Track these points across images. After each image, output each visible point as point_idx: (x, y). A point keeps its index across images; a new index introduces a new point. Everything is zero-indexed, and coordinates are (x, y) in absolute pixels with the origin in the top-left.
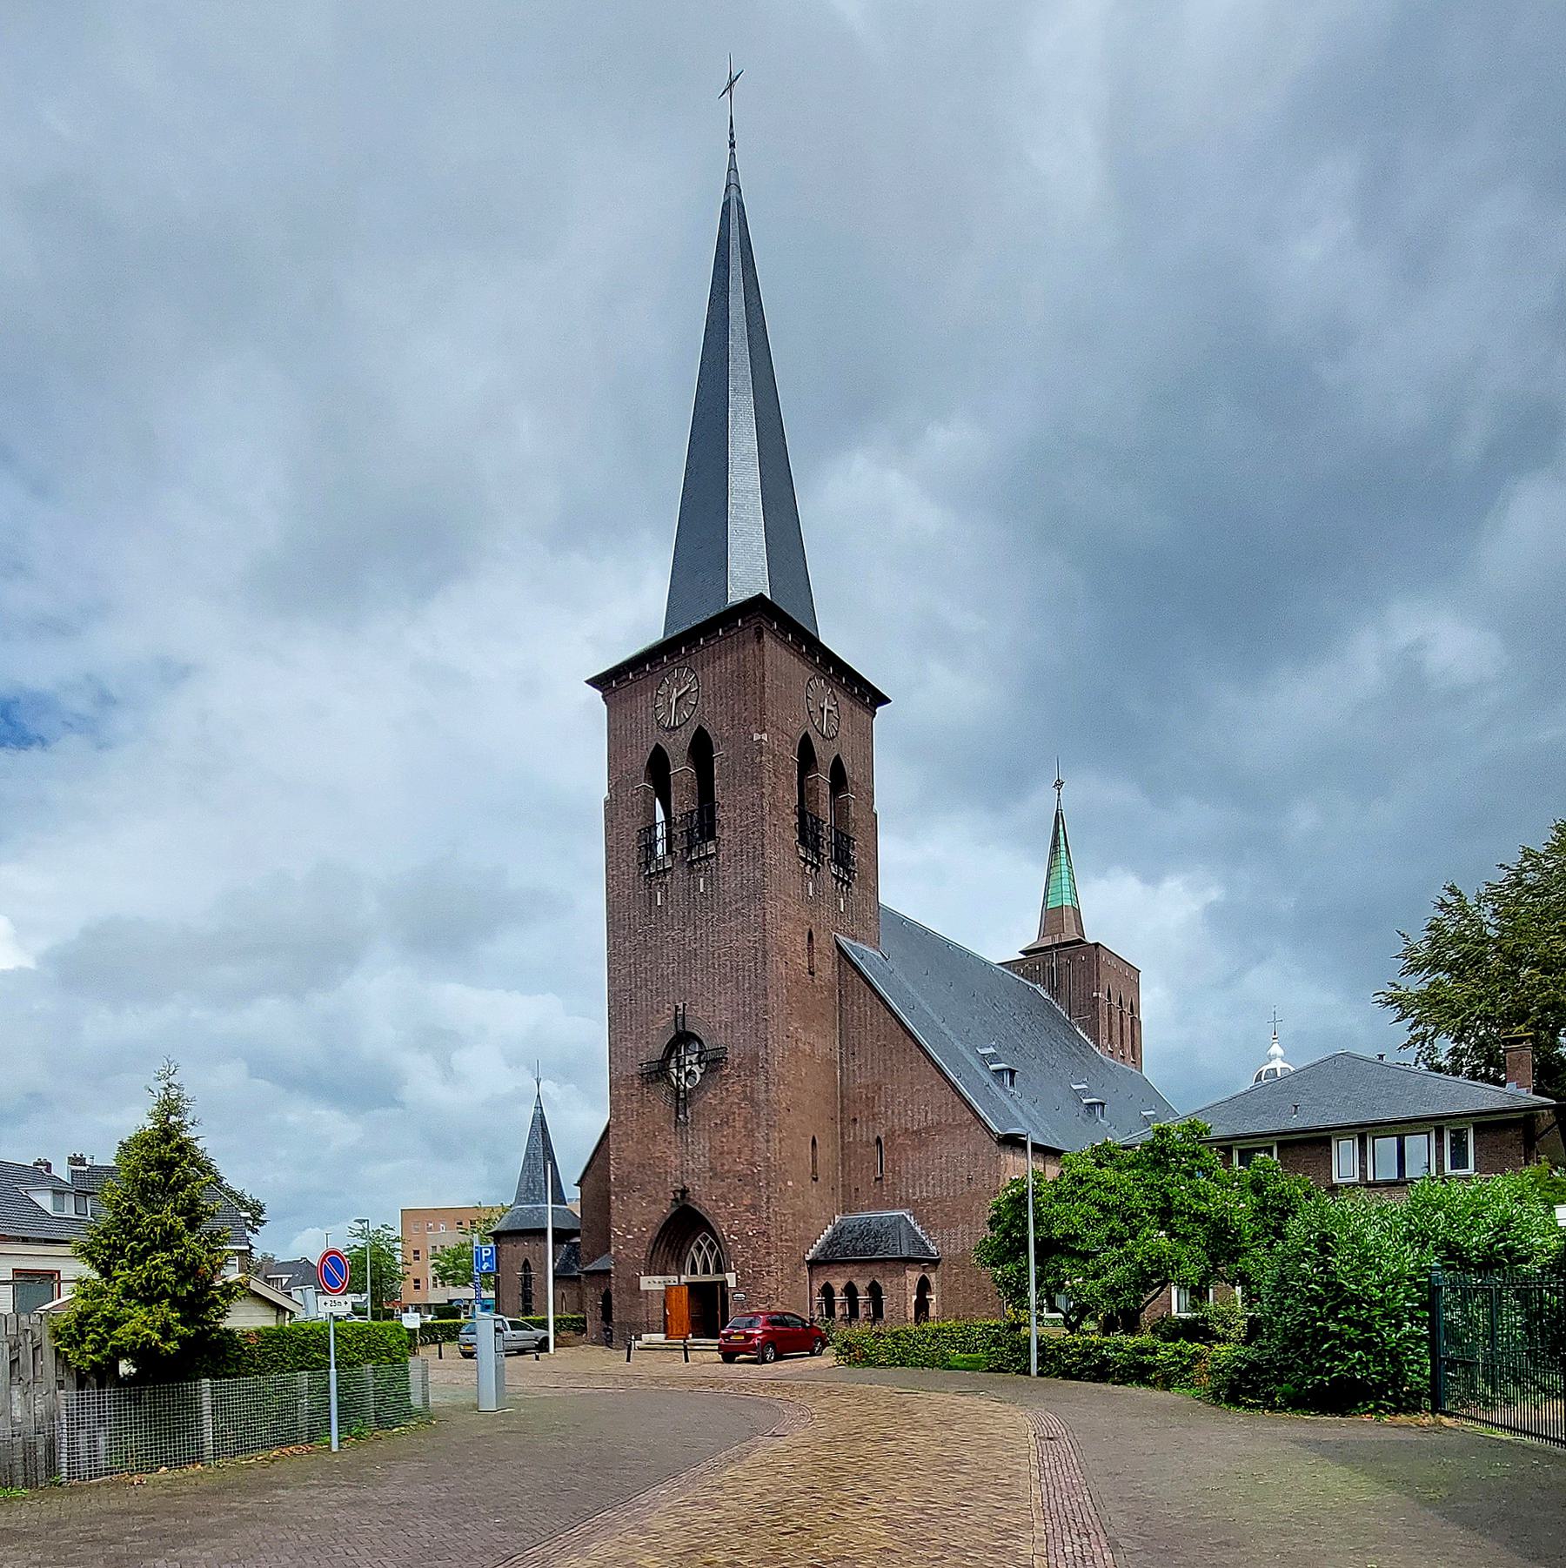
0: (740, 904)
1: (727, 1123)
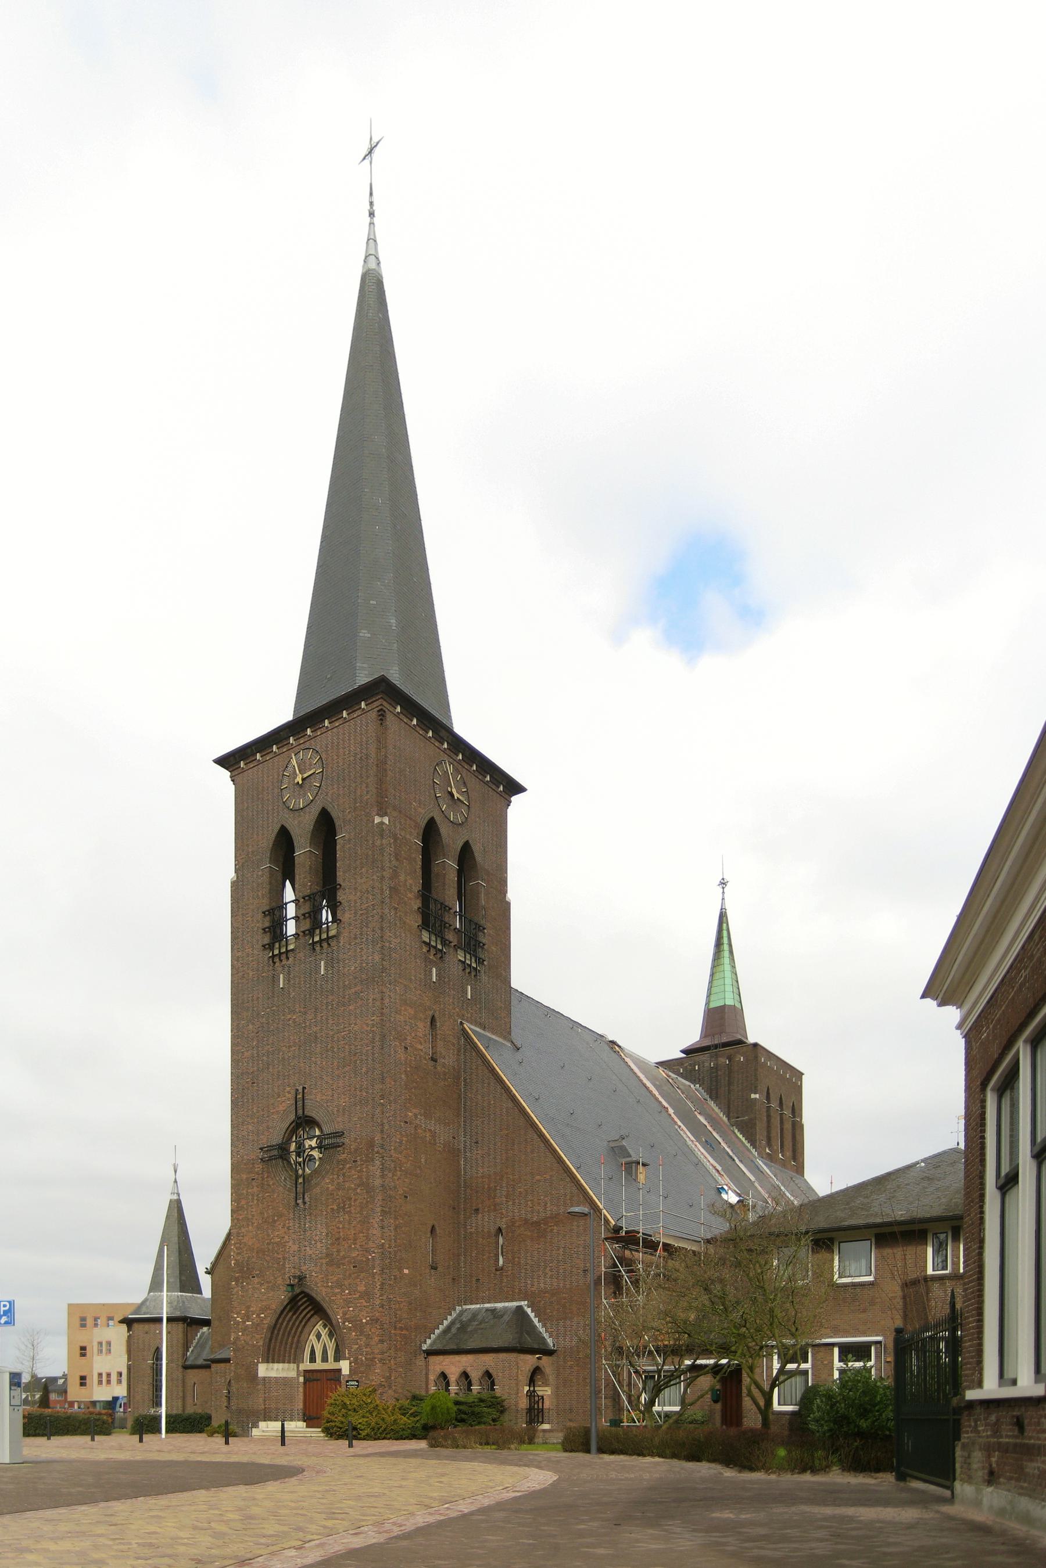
0: (359, 988)
1: (344, 1208)
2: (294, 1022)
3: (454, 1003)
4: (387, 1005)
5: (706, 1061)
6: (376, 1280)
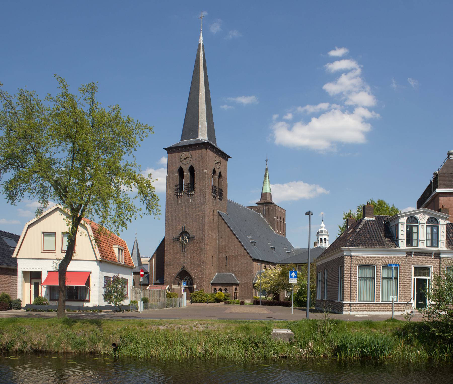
0: (199, 205)
1: (195, 252)
2: (183, 210)
5: (262, 207)
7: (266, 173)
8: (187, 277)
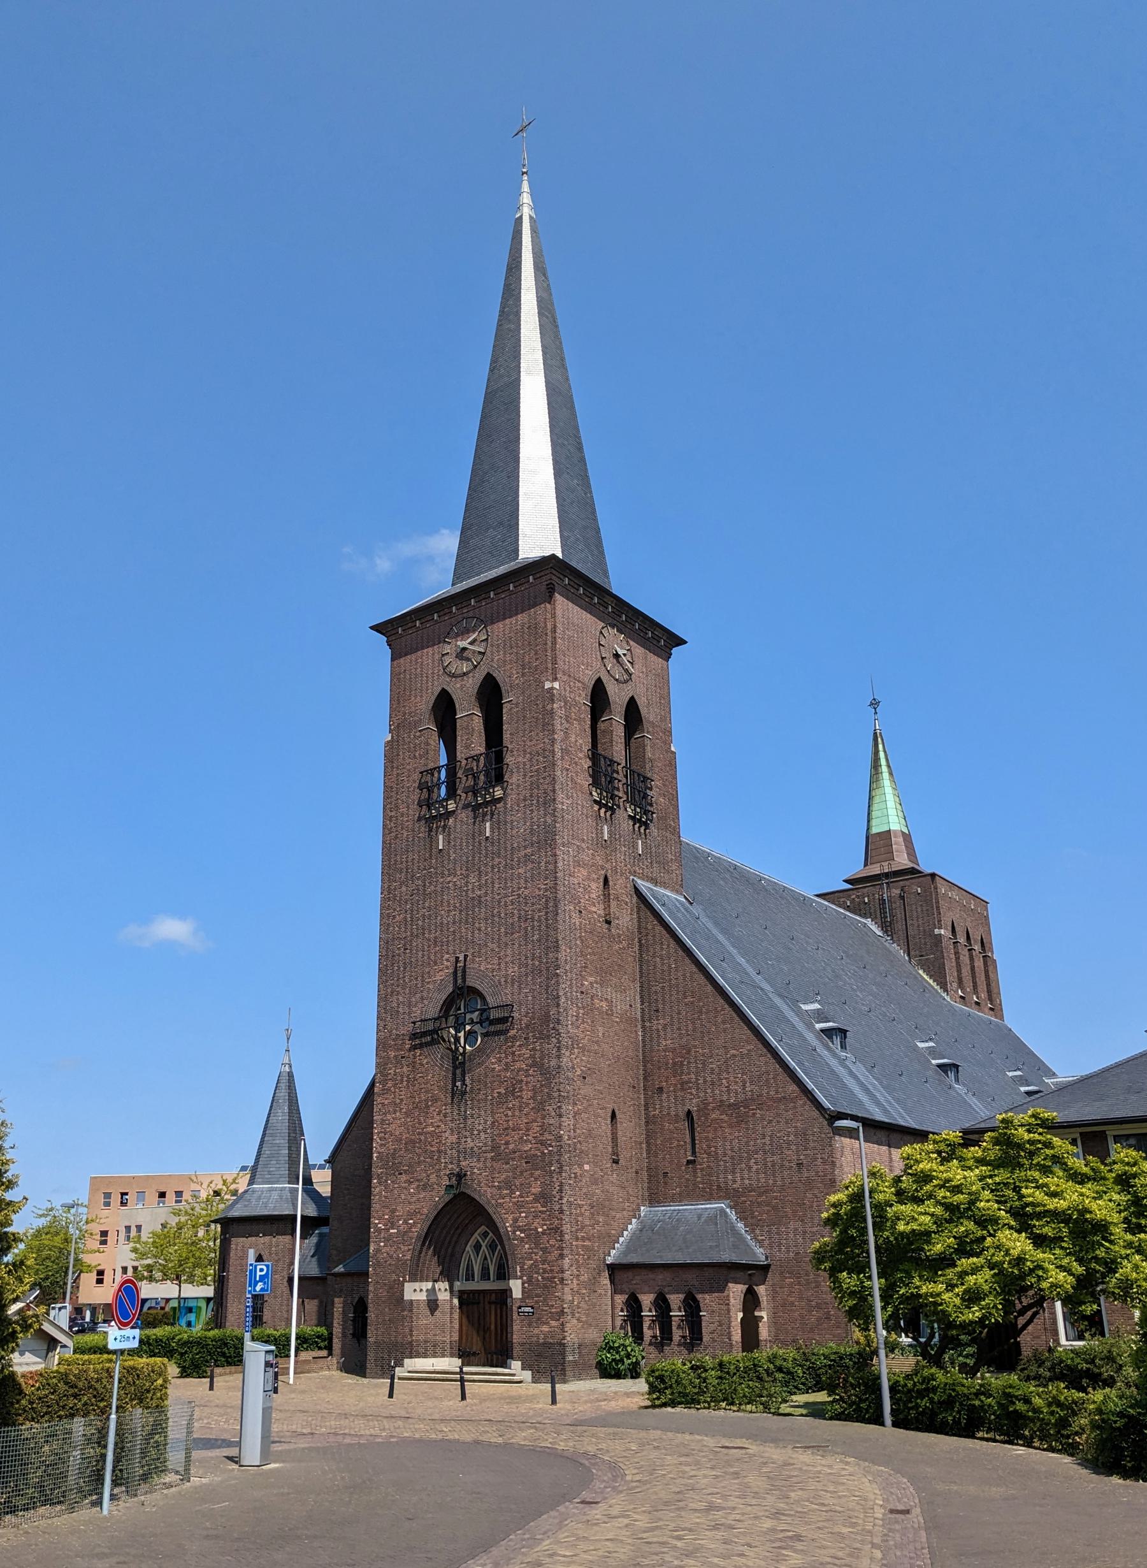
3: (625, 860)
4: (560, 868)
5: (868, 894)
6: (555, 1180)
7: (876, 752)
8: (485, 1235)
